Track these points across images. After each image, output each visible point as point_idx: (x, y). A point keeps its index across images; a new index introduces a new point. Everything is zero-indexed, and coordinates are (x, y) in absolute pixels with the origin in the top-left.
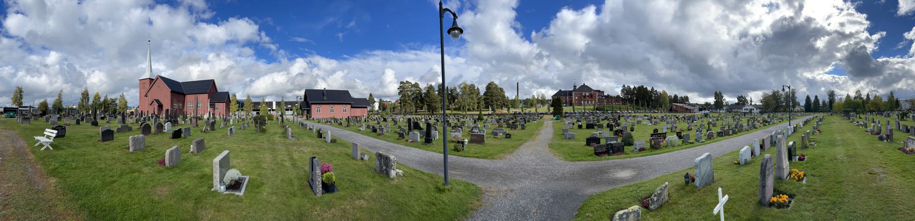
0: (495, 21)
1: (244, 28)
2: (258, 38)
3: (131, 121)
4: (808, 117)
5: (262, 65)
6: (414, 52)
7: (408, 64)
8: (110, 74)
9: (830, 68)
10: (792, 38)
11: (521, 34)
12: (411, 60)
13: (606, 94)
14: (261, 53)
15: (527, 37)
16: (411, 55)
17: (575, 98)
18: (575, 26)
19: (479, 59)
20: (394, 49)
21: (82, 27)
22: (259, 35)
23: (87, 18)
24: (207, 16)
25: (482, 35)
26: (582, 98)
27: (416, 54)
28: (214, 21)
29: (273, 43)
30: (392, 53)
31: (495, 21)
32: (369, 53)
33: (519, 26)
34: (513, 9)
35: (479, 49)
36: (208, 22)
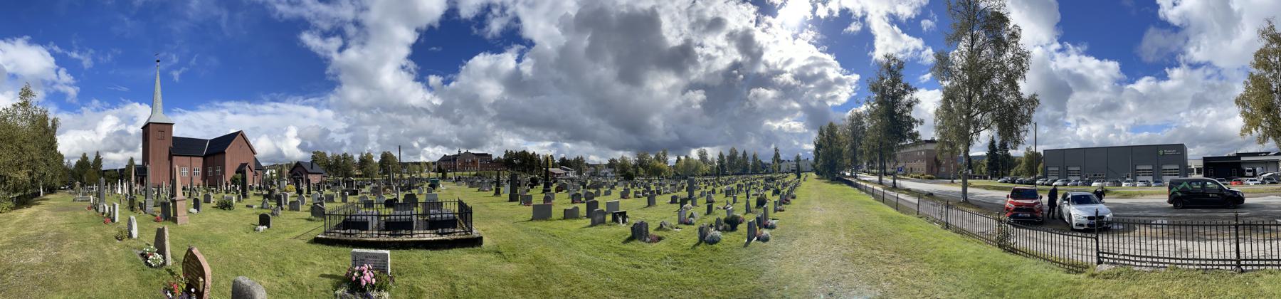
2: (54, 76)
7: (261, 119)
12: (264, 114)
15: (421, 78)
16: (268, 107)
17: (458, 164)
18: (486, 74)
19: (341, 109)
22: (57, 71)
25: (363, 77)
29: (76, 85)
30: (248, 106)
31: (386, 68)
33: (412, 65)
34: (417, 30)
35: (354, 94)
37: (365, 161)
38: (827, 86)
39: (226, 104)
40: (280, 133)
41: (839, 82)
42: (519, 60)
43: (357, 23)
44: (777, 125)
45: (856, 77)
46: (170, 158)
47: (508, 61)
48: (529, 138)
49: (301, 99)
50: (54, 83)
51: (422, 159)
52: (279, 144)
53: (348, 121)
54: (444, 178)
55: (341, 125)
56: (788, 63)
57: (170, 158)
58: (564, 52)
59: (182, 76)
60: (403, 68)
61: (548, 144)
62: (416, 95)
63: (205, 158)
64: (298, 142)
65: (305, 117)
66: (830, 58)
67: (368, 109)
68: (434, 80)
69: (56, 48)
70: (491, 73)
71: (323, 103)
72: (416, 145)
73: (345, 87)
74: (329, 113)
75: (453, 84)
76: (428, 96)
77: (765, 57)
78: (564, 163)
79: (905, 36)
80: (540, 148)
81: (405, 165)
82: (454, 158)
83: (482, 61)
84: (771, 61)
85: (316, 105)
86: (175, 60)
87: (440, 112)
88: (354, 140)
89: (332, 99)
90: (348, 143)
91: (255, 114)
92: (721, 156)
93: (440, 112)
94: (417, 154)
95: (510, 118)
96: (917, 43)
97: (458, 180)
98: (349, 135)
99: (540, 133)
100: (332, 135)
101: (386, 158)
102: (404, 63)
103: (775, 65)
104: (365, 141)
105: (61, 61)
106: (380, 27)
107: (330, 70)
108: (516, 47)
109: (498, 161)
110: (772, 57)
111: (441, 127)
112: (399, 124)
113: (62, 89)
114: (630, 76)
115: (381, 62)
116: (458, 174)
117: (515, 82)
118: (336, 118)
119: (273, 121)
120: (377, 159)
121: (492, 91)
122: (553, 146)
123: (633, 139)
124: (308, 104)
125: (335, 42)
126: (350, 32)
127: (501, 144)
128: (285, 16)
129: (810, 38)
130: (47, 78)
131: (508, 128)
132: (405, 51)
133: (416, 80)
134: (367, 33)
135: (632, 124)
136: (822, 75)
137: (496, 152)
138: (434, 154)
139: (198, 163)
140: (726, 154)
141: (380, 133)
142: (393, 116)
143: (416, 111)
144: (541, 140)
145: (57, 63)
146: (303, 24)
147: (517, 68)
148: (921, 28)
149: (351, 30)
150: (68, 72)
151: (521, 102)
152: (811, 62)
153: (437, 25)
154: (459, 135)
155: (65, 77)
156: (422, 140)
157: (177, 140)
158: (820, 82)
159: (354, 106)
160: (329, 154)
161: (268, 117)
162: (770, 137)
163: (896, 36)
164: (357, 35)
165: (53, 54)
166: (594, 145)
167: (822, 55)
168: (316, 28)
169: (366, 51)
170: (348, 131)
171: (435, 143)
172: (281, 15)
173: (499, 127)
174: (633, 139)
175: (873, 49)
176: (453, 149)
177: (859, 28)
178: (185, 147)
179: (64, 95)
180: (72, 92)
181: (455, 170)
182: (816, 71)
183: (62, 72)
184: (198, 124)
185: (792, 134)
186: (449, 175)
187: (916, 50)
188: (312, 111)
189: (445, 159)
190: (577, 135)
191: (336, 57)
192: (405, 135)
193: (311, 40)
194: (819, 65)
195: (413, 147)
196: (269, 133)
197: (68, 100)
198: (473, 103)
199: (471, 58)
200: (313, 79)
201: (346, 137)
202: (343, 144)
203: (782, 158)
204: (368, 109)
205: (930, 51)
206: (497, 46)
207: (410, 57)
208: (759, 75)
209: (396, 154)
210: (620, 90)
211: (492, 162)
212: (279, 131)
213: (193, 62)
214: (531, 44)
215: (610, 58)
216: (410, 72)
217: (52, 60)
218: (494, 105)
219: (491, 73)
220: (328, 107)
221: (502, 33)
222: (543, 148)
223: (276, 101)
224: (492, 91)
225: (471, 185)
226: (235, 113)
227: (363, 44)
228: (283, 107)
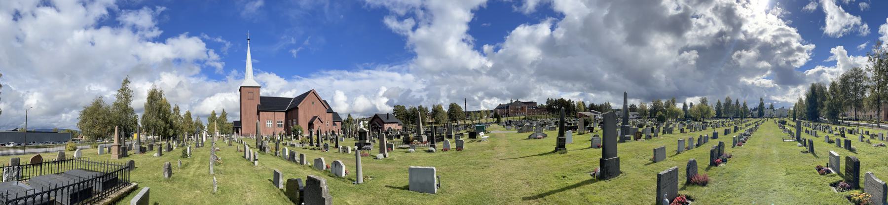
0: (448, 38)
1: (191, 46)
2: (205, 56)
3: (394, 126)
4: (55, 118)
5: (211, 85)
6: (367, 71)
7: (359, 83)
8: (49, 96)
9: (764, 76)
10: (721, 51)
11: (471, 47)
12: (361, 79)
13: (538, 104)
14: (209, 72)
15: (478, 47)
16: (363, 74)
17: (511, 110)
18: (527, 41)
19: (420, 73)
20: (350, 68)
21: (19, 45)
22: (207, 52)
23: (25, 36)
24: (156, 33)
25: (434, 49)
26: (516, 112)
27: (369, 73)
28: (162, 40)
29: (220, 61)
30: (346, 73)
31: (448, 38)
32: (324, 72)
33: (470, 38)
34: (472, 11)
35: (428, 62)
36: (155, 40)
37: (437, 111)
38: (790, 53)
39: (332, 72)
40: (372, 94)
41: (800, 50)
42: (552, 29)
43: (423, 9)
44: (749, 81)
45: (812, 46)
46: (258, 114)
47: (544, 30)
48: (563, 90)
49: (387, 66)
50: (205, 61)
51: (483, 108)
52: (373, 102)
53: (424, 83)
54: (498, 122)
55: (420, 86)
56: (761, 33)
57: (258, 114)
58: (588, 21)
59: (298, 53)
60: (463, 40)
61: (577, 94)
62: (475, 61)
63: (287, 112)
64: (386, 100)
65: (392, 80)
66: (793, 31)
67: (439, 73)
68: (486, 48)
69: (206, 37)
70: (530, 40)
71: (404, 69)
72: (476, 98)
73: (420, 57)
74: (410, 77)
75: (500, 51)
76: (484, 60)
77: (744, 27)
78: (592, 107)
79: (848, 15)
80: (573, 96)
81: (468, 114)
82: (507, 106)
83: (522, 31)
84: (750, 31)
85: (399, 71)
86: (293, 41)
87: (493, 72)
88: (429, 96)
89: (412, 67)
90: (425, 98)
91: (354, 80)
92: (719, 103)
93: (493, 72)
94: (478, 105)
95: (544, 72)
96: (857, 20)
97: (509, 124)
98: (427, 92)
99: (569, 85)
100: (412, 94)
101: (453, 108)
102: (464, 37)
103: (752, 35)
104: (438, 97)
105: (210, 45)
106: (442, 11)
107: (408, 44)
108: (550, 19)
109: (542, 107)
110: (750, 28)
111: (495, 85)
112: (464, 83)
113: (213, 64)
114: (636, 38)
115: (446, 36)
116: (510, 118)
117: (550, 46)
118: (416, 81)
119: (367, 84)
120: (446, 109)
121: (532, 53)
122: (581, 95)
123: (643, 90)
124: (393, 71)
125: (409, 23)
126: (421, 15)
127: (540, 95)
128: (372, 6)
129: (779, 13)
130: (201, 59)
131: (543, 81)
132: (464, 28)
133: (474, 49)
134: (432, 15)
135: (641, 77)
136: (787, 44)
137: (541, 102)
138: (493, 103)
139: (281, 116)
140: (723, 102)
141: (449, 90)
142: (457, 77)
143: (477, 72)
144: (572, 90)
145: (207, 47)
146: (384, 11)
147: (551, 35)
148: (859, 9)
149: (421, 13)
150: (215, 52)
151: (556, 61)
152: (778, 33)
153: (485, 6)
154: (508, 89)
155: (213, 56)
156: (480, 94)
157: (263, 99)
158: (786, 49)
159: (429, 72)
160: (407, 108)
161: (365, 82)
162: (747, 90)
163: (842, 15)
164: (425, 17)
165: (204, 40)
166: (612, 94)
167: (788, 28)
168: (393, 14)
169: (433, 29)
170: (425, 90)
171: (491, 95)
172: (369, 6)
173: (538, 81)
174: (643, 90)
175: (824, 24)
176: (505, 99)
177: (814, 8)
178: (269, 104)
179: (214, 68)
180: (219, 66)
181: (508, 115)
182: (783, 40)
183: (211, 52)
184: (276, 86)
185: (763, 88)
186: (504, 120)
187: (856, 25)
188: (397, 76)
189: (501, 107)
190: (598, 87)
191: (410, 34)
192: (467, 91)
193: (391, 23)
194: (786, 36)
195: (474, 100)
196: (366, 94)
197: (216, 72)
198: (514, 62)
199: (514, 29)
200: (394, 51)
201: (424, 95)
202: (422, 100)
203: (407, 183)
204: (439, 73)
205: (866, 26)
206: (533, 19)
207: (468, 32)
208: (740, 41)
209: (462, 106)
210: (629, 50)
211: (537, 108)
212: (359, 93)
213: (307, 42)
214: (561, 16)
215: (620, 25)
216: (469, 43)
217: (204, 44)
218: (533, 64)
219: (530, 40)
220: (408, 71)
221: (537, 7)
222: (573, 97)
223: (369, 69)
224: (532, 53)
225: (521, 129)
226: (339, 79)
227: (430, 24)
228: (375, 73)
